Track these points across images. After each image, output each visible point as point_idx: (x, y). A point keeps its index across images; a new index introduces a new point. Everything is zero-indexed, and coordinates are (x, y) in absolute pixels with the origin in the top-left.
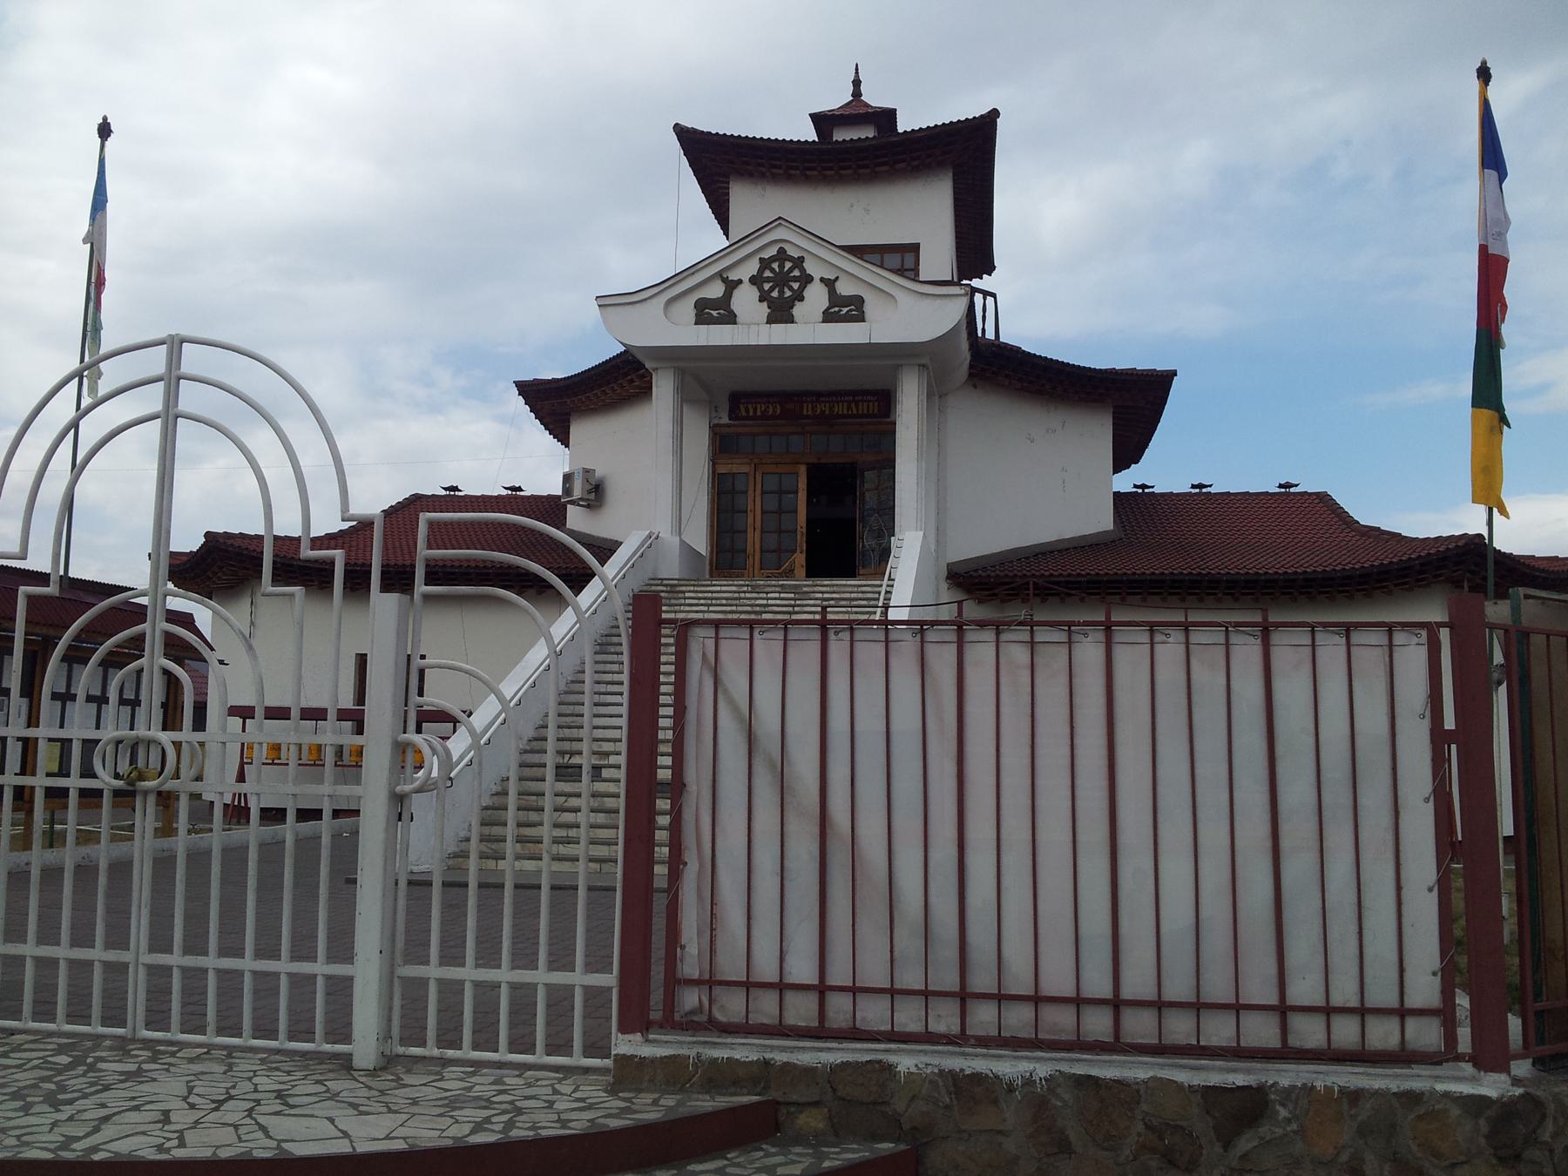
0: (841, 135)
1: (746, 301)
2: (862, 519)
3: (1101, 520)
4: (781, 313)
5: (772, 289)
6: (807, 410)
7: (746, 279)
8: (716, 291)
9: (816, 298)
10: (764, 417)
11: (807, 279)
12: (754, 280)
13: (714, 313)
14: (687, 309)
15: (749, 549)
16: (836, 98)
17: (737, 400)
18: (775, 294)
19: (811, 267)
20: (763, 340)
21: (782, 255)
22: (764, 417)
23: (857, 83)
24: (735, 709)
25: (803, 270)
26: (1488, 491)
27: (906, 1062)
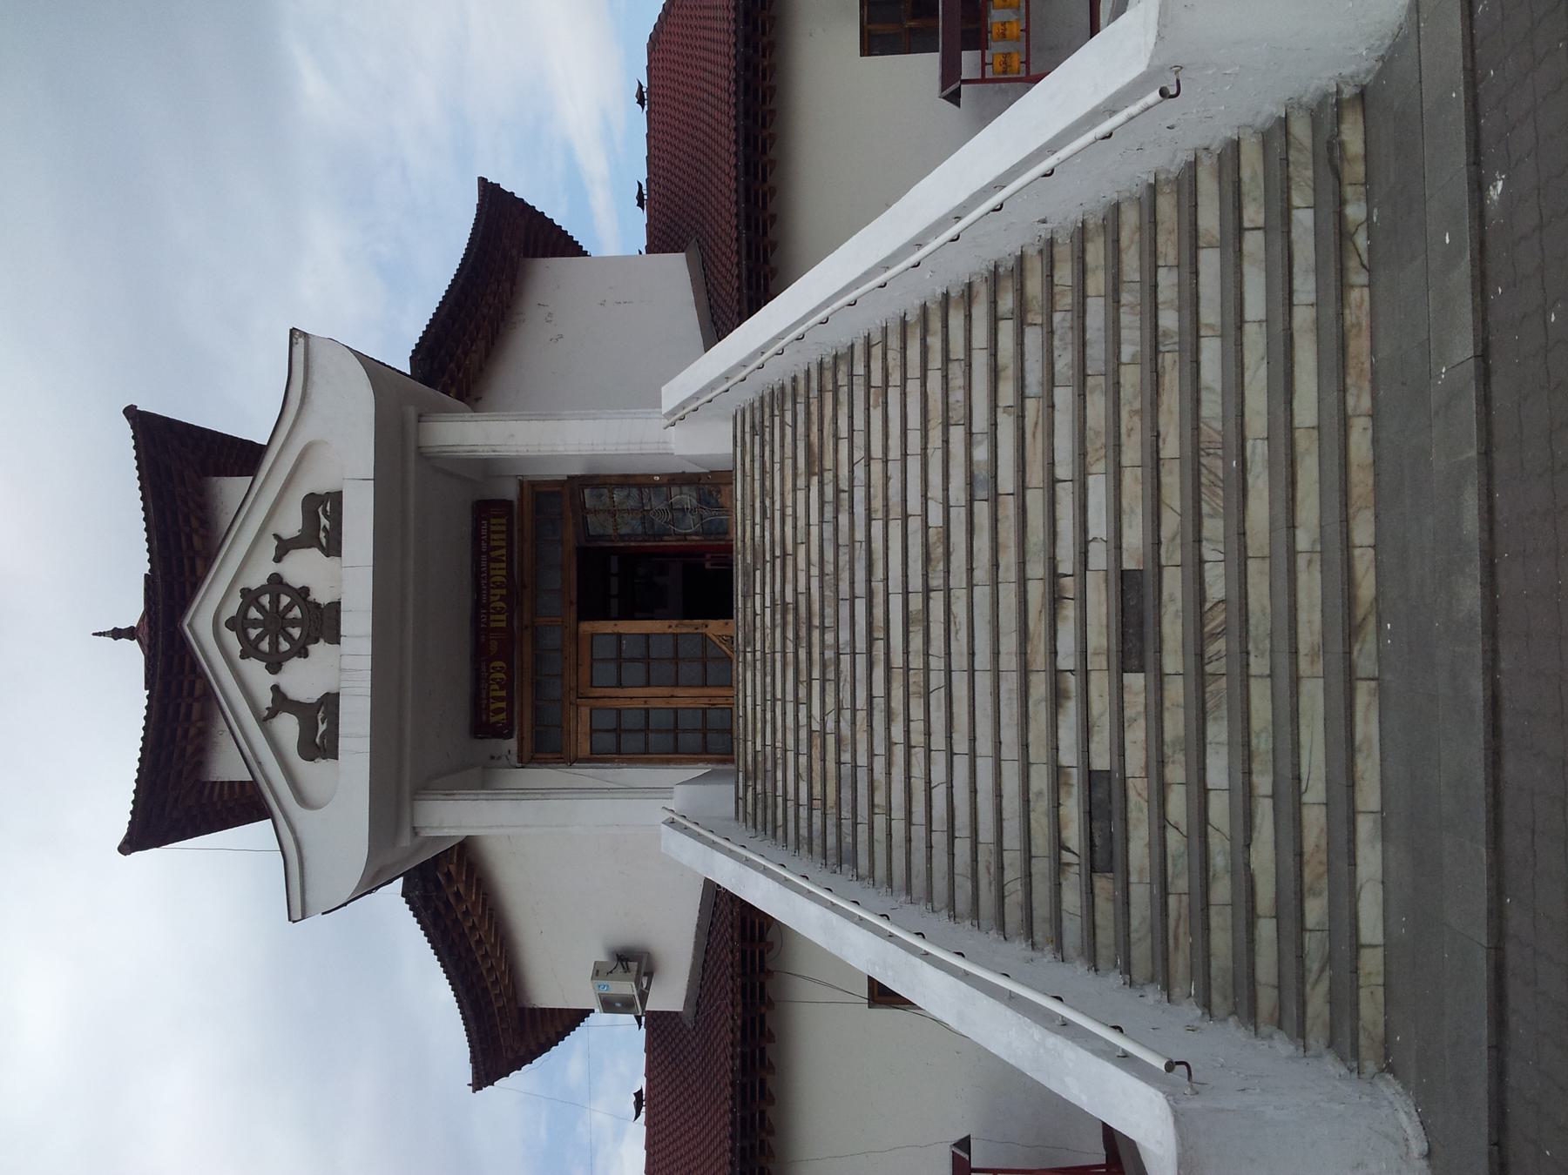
1: (305, 678)
2: (659, 536)
3: (676, 266)
4: (323, 623)
5: (289, 638)
7: (272, 679)
8: (288, 727)
9: (304, 568)
10: (508, 685)
11: (276, 581)
12: (274, 667)
13: (322, 728)
14: (313, 773)
15: (702, 703)
17: (482, 728)
18: (296, 632)
19: (257, 578)
20: (366, 646)
21: (239, 624)
22: (508, 685)
23: (117, 634)
25: (262, 590)
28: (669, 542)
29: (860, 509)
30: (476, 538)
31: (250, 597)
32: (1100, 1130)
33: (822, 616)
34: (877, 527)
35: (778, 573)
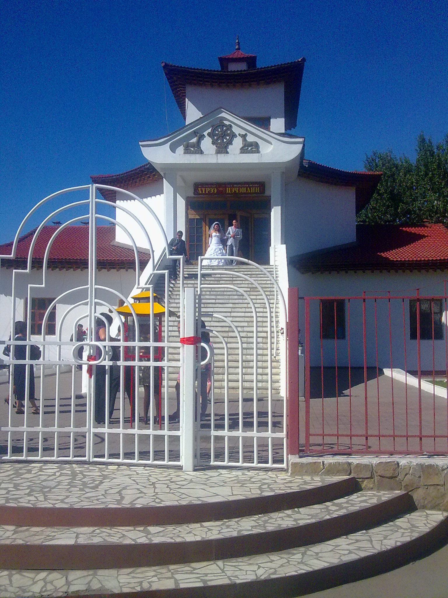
0: (233, 67)
1: (207, 144)
4: (222, 149)
5: (217, 139)
6: (228, 190)
9: (238, 142)
11: (234, 136)
12: (209, 134)
14: (181, 149)
19: (235, 129)
26: (367, 430)
27: (403, 461)
29: (237, 301)
32: (8, 242)
33: (213, 291)
34: (231, 305)
35: (228, 279)
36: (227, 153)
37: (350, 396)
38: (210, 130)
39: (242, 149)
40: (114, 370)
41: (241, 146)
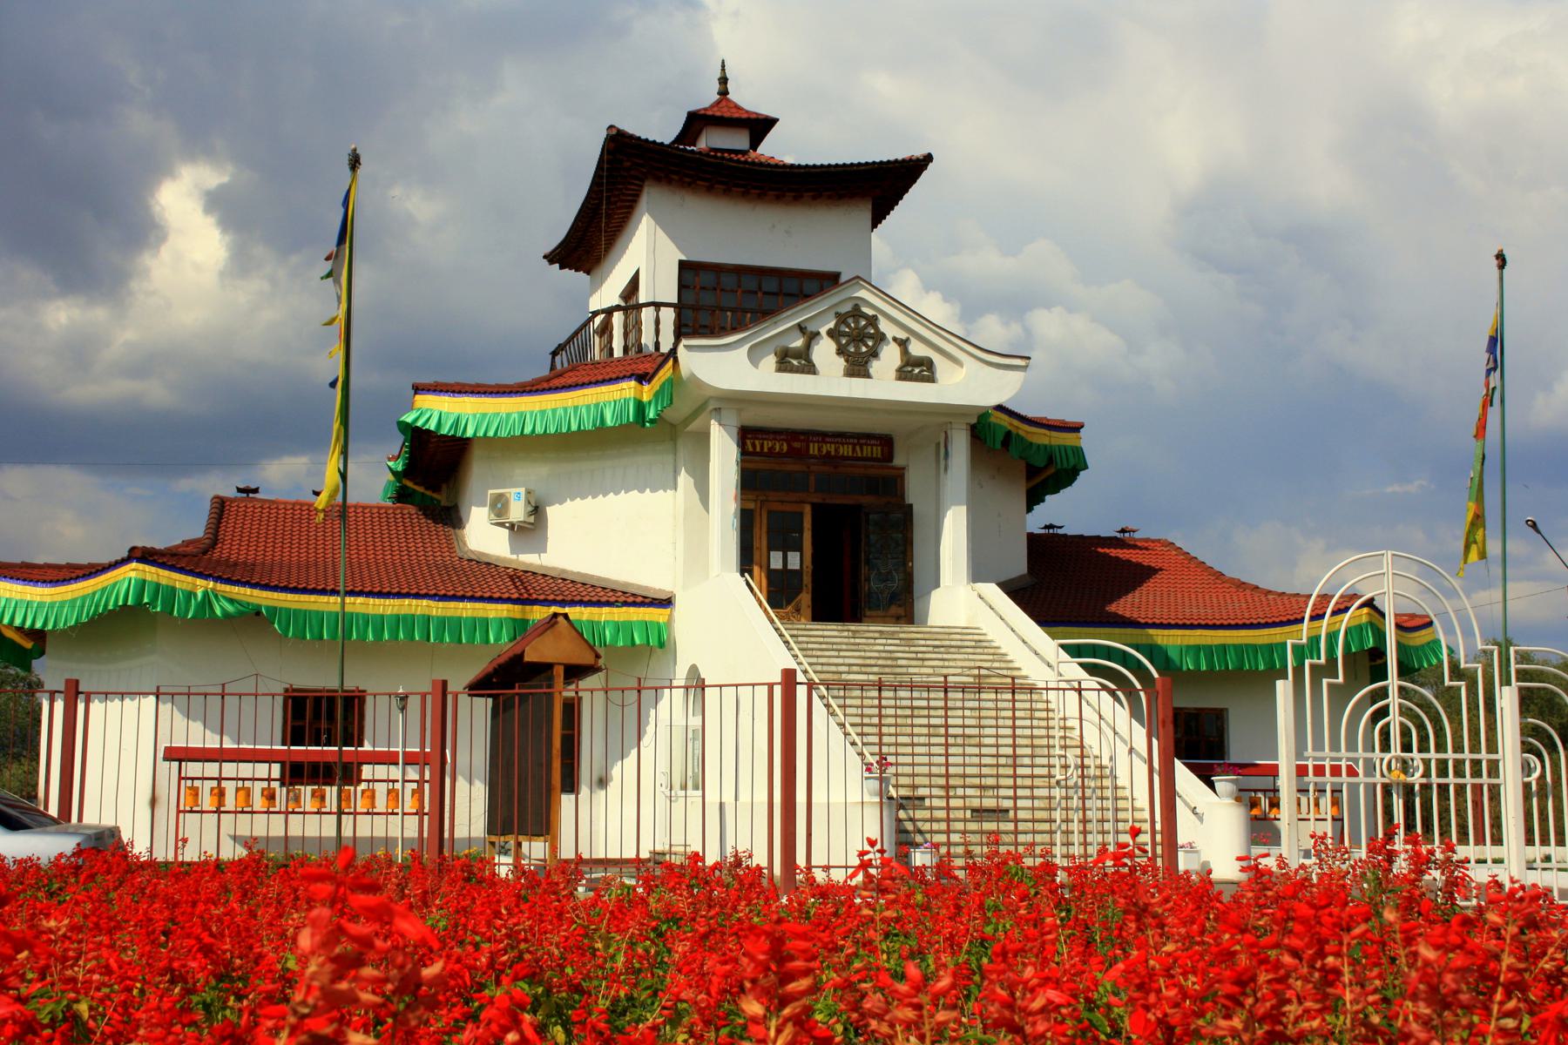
1: (825, 352)
4: (858, 367)
5: (848, 344)
6: (813, 449)
7: (823, 331)
8: (798, 343)
9: (890, 357)
11: (881, 338)
12: (831, 333)
14: (770, 361)
16: (706, 97)
19: (885, 326)
23: (724, 80)
24: (1139, 755)
25: (877, 329)
28: (864, 569)
30: (869, 436)
31: (873, 321)
36: (868, 376)
37: (218, 812)
38: (832, 325)
39: (899, 370)
40: (1426, 788)
41: (897, 363)
